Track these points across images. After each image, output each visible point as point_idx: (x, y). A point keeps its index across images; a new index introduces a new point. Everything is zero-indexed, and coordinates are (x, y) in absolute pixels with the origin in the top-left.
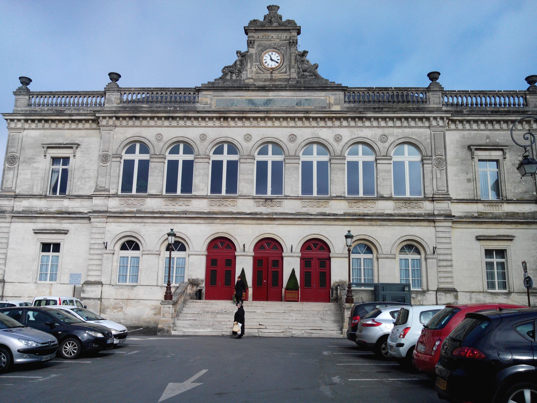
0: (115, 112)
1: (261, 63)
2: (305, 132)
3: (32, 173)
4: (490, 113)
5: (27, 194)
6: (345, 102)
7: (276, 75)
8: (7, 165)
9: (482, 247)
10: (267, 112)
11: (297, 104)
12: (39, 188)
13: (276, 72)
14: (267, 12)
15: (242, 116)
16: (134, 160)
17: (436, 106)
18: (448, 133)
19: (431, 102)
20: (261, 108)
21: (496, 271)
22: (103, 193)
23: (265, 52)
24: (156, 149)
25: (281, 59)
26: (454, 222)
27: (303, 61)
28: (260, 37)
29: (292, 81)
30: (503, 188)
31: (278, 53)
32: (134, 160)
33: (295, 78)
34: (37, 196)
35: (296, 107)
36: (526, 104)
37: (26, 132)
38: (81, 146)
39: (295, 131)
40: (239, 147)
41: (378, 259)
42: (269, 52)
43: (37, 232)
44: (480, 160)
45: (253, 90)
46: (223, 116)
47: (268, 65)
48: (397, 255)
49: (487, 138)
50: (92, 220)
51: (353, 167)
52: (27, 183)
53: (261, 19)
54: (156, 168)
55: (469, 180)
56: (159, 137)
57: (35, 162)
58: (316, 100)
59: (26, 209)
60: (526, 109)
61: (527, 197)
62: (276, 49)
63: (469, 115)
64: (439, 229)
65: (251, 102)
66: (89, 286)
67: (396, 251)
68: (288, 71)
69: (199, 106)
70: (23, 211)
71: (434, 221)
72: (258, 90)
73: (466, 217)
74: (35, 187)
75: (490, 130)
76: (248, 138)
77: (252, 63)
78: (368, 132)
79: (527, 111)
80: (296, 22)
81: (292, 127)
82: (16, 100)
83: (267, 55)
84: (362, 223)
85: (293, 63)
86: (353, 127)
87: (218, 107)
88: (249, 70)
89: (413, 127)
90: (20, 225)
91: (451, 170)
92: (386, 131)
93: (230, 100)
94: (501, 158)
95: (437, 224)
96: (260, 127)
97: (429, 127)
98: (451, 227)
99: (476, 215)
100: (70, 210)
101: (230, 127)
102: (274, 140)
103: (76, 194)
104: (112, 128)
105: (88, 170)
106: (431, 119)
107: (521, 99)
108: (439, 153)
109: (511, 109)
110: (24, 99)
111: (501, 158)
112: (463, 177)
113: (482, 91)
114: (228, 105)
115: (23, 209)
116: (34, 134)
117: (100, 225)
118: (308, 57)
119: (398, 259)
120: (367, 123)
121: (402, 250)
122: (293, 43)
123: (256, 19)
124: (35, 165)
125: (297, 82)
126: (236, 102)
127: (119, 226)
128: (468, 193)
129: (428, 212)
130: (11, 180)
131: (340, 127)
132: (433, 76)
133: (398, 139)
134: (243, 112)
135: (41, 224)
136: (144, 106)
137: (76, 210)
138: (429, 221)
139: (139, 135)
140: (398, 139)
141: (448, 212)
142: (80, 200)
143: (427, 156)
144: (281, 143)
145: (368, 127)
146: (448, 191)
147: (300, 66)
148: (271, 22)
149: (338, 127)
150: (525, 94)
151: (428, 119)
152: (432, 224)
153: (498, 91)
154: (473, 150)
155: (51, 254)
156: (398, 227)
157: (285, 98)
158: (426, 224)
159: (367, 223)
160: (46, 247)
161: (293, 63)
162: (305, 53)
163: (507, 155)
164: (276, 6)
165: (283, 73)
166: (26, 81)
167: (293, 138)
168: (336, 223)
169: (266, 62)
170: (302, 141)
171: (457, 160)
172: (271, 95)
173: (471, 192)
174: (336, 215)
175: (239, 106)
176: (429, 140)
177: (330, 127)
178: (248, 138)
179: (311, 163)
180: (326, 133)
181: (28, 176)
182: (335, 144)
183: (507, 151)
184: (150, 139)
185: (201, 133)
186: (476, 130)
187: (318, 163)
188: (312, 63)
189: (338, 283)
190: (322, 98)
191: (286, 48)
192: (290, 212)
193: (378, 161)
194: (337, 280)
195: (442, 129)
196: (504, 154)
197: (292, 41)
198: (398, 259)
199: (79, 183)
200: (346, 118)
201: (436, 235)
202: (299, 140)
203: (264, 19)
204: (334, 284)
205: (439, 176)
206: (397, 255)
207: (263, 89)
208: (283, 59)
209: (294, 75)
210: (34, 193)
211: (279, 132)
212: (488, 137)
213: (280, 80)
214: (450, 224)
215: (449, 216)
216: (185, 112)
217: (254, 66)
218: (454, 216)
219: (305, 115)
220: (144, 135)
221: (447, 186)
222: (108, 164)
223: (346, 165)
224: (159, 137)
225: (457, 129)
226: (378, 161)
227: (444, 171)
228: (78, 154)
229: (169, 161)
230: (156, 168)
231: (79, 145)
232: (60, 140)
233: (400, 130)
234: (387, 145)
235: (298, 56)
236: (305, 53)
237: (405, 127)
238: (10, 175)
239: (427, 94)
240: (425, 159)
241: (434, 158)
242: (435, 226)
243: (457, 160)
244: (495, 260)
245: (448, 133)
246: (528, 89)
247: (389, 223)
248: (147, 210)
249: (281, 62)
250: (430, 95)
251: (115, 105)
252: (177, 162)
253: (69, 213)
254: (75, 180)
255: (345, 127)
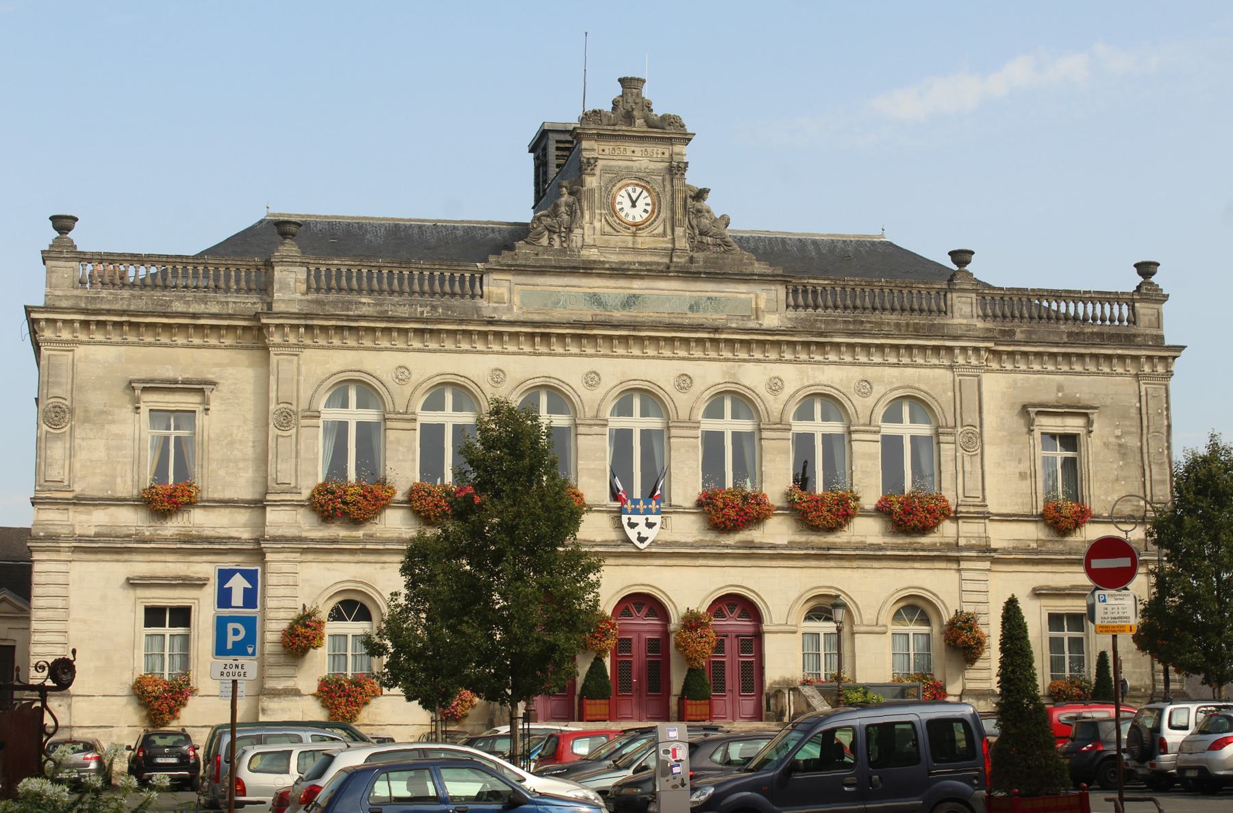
0: (306, 316)
1: (614, 213)
2: (709, 373)
3: (108, 448)
4: (1065, 339)
5: (101, 495)
6: (788, 306)
7: (644, 240)
8: (45, 428)
9: (1044, 609)
10: (634, 326)
11: (691, 308)
12: (130, 482)
13: (644, 233)
14: (618, 90)
15: (582, 334)
16: (631, 431)
17: (964, 321)
18: (987, 379)
19: (956, 314)
20: (618, 315)
21: (1067, 655)
22: (288, 497)
23: (619, 185)
24: (397, 401)
25: (654, 204)
26: (995, 561)
27: (699, 211)
28: (607, 152)
29: (679, 257)
30: (1085, 493)
31: (648, 190)
32: (631, 431)
33: (684, 250)
34: (125, 499)
35: (690, 315)
36: (1133, 320)
37: (80, 351)
38: (220, 387)
39: (688, 367)
40: (575, 399)
41: (853, 634)
42: (628, 185)
43: (133, 583)
44: (235, 682)
45: (599, 275)
46: (541, 334)
47: (627, 215)
48: (889, 625)
49: (1059, 391)
50: (269, 557)
51: (804, 443)
52: (98, 471)
53: (607, 107)
54: (398, 441)
55: (1022, 476)
56: (403, 373)
57: (113, 422)
58: (728, 299)
59: (103, 530)
60: (1133, 330)
61: (1127, 509)
62: (643, 180)
63: (1027, 343)
64: (965, 575)
65: (596, 300)
66: (276, 699)
67: (886, 617)
68: (669, 231)
69: (486, 307)
70: (97, 535)
71: (957, 560)
72: (611, 276)
73: (1015, 550)
74: (119, 480)
75: (1066, 373)
76: (592, 379)
77: (591, 208)
78: (833, 374)
79: (1135, 336)
80: (684, 121)
81: (684, 359)
82: (49, 272)
83: (623, 192)
84: (823, 563)
85: (679, 215)
86: (805, 362)
87: (525, 309)
88: (586, 226)
89: (921, 366)
90: (92, 567)
91: (992, 453)
92: (870, 372)
93: (551, 294)
94: (1082, 431)
95: (964, 565)
96: (617, 357)
97: (951, 367)
98: (989, 570)
99: (1034, 545)
100: (208, 533)
101: (555, 355)
102: (645, 386)
103: (217, 496)
104: (295, 351)
105: (241, 441)
106: (957, 351)
107: (1125, 307)
108: (970, 421)
109: (1106, 330)
110: (69, 270)
111: (1082, 431)
112: (1013, 468)
113: (1052, 291)
114: (545, 305)
115: (97, 529)
116: (101, 359)
117: (286, 567)
118: (709, 202)
119: (889, 633)
120: (832, 357)
121: (897, 616)
122: (676, 169)
123: (597, 108)
124: (115, 429)
125: (691, 260)
126: (563, 299)
127: (329, 570)
128: (1020, 500)
129: (947, 540)
130: (60, 462)
131: (780, 360)
132: (961, 257)
133: (892, 390)
134: (584, 325)
135: (141, 567)
136: (364, 300)
137: (223, 533)
138: (948, 559)
139: (358, 368)
140: (892, 390)
141: (983, 542)
142: (228, 510)
143: (947, 427)
144: (660, 393)
145: (834, 363)
146: (984, 499)
147: (694, 222)
148: (629, 118)
149: (775, 361)
150: (1133, 301)
151: (950, 349)
152: (955, 566)
153: (1085, 292)
154: (1033, 415)
155: (167, 631)
156: (891, 571)
157: (668, 297)
158: (943, 565)
159: (832, 563)
160: (154, 616)
161: (679, 215)
162: (701, 195)
163: (1095, 426)
164: (638, 80)
165: (658, 235)
166: (63, 224)
167: (684, 382)
168: (774, 563)
169: (622, 209)
170: (703, 389)
171: (1001, 434)
172: (637, 286)
173: (1028, 500)
174: (774, 547)
175: (570, 306)
176: (950, 394)
177: (759, 361)
178: (592, 379)
179: (441, 427)
180: (754, 375)
181: (101, 454)
182: (769, 397)
183: (1094, 417)
184: (384, 378)
185: (494, 367)
186: (1038, 372)
187: (360, 425)
188: (717, 214)
189: (778, 683)
190: (743, 296)
191: (663, 180)
192: (683, 539)
193: (765, 434)
194: (777, 678)
195: (975, 372)
196: (1090, 423)
197: (675, 164)
198: (889, 633)
199: (222, 472)
200: (792, 344)
201: (960, 586)
202: (698, 386)
203: (613, 109)
204: (771, 687)
205: (968, 468)
206: (889, 625)
207: (619, 272)
208: (657, 205)
209: (682, 243)
210: (119, 495)
211: (656, 370)
212: (1060, 388)
213: (653, 251)
214: (987, 565)
215: (985, 552)
216: (461, 322)
217: (598, 217)
218: (995, 550)
219: (712, 336)
220: (368, 367)
221: (983, 489)
222: (293, 431)
223: (607, 437)
224: (403, 373)
225: (1002, 370)
226: (942, 438)
227: (978, 458)
228: (214, 405)
229: (424, 427)
230: (398, 441)
231: (215, 384)
232: (168, 372)
233: (895, 371)
234: (871, 401)
235: (689, 200)
236: (701, 195)
237: (906, 366)
238: (57, 451)
239: (949, 295)
240: (943, 433)
241: (960, 430)
242: (959, 570)
243: (1001, 434)
244: (1066, 634)
245: (987, 379)
246: (1139, 287)
247: (876, 564)
248: (387, 535)
249: (653, 211)
250: (955, 300)
251: (298, 296)
252: (441, 427)
253: (208, 540)
254: (214, 466)
255: (790, 362)
